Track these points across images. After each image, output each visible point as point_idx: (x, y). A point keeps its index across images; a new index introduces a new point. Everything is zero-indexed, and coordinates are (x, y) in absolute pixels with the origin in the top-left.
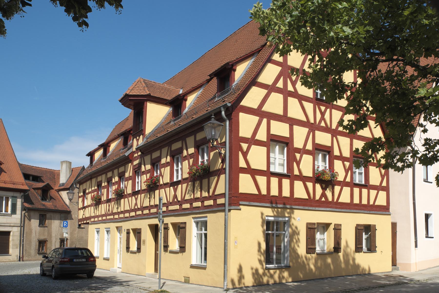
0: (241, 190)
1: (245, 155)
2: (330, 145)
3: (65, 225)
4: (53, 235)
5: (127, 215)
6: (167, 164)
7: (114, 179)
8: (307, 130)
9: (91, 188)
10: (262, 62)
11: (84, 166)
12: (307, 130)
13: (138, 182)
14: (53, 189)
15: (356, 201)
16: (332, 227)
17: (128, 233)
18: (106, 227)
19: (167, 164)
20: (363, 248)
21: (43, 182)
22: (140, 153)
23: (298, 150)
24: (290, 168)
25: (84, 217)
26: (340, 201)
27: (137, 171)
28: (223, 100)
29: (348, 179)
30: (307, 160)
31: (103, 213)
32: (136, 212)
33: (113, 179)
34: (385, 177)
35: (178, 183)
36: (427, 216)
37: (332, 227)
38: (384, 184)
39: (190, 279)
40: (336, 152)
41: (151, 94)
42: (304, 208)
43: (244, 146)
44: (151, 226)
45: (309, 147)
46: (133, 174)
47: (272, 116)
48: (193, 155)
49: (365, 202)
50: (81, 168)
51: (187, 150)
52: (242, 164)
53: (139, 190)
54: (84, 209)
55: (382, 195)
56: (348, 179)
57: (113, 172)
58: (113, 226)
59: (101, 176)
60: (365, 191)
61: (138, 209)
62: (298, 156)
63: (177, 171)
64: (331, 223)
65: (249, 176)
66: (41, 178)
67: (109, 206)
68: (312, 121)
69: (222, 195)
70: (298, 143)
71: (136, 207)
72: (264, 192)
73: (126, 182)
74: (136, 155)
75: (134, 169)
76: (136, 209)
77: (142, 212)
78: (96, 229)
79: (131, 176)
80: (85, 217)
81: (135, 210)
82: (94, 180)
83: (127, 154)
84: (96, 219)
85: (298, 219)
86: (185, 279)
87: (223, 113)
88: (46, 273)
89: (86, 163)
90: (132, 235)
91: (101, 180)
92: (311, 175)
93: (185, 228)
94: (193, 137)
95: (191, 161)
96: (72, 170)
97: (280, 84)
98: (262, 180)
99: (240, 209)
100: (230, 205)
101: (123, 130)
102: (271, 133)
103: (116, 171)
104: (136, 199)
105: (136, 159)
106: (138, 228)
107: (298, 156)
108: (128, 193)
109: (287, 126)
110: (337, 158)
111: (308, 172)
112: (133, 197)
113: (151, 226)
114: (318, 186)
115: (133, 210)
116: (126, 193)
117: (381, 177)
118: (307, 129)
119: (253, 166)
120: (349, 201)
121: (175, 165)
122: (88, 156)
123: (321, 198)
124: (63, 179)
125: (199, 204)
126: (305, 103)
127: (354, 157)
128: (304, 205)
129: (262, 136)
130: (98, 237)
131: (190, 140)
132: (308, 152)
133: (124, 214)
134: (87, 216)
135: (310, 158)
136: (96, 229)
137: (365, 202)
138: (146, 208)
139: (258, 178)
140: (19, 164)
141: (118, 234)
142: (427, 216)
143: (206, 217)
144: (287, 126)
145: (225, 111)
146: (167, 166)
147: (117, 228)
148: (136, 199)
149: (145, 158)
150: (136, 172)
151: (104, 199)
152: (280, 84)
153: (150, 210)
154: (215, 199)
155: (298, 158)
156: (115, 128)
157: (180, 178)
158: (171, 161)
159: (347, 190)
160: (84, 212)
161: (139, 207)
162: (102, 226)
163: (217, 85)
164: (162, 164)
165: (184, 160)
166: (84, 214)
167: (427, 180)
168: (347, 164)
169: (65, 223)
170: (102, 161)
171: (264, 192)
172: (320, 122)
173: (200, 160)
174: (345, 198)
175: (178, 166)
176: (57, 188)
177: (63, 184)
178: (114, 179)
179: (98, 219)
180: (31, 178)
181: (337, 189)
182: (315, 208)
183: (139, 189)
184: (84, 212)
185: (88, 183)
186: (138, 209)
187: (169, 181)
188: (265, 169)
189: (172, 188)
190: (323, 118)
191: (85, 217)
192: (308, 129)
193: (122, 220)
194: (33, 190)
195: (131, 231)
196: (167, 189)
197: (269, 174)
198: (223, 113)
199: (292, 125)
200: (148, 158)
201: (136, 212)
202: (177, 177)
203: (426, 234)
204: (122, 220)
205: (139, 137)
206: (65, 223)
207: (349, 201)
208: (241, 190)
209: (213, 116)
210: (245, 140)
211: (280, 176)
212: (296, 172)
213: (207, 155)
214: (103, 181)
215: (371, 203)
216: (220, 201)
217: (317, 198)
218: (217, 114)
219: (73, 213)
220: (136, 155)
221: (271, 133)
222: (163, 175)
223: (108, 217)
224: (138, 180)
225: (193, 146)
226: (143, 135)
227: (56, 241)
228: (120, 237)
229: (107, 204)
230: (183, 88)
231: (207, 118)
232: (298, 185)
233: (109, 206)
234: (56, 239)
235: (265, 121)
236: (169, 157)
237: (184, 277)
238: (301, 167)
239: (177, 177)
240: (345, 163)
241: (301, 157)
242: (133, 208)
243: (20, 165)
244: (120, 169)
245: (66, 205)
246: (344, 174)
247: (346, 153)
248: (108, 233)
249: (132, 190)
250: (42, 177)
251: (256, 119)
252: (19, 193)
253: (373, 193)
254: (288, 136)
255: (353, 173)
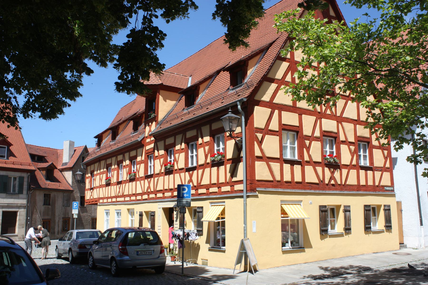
1: (260, 143)
2: (336, 131)
3: (75, 207)
4: (57, 214)
5: (139, 197)
6: (182, 150)
7: (125, 162)
9: (100, 170)
10: (273, 60)
11: (86, 146)
12: (314, 118)
13: (151, 166)
14: (57, 168)
15: (363, 182)
17: (141, 215)
18: (116, 209)
19: (182, 150)
20: (372, 228)
21: (47, 162)
22: (153, 139)
23: (307, 137)
24: (301, 155)
25: (92, 198)
26: (347, 183)
27: (150, 155)
28: (237, 93)
29: (354, 162)
30: (316, 146)
31: (113, 195)
32: (148, 195)
33: (124, 162)
35: (193, 169)
39: (208, 261)
40: (342, 138)
41: (164, 84)
43: (260, 136)
44: (165, 209)
45: (317, 134)
46: (145, 158)
47: (282, 108)
48: (208, 143)
50: (84, 147)
51: (202, 138)
52: (258, 153)
53: (153, 174)
54: (91, 191)
56: (354, 162)
57: (124, 156)
58: (124, 208)
59: (110, 159)
60: (370, 173)
61: (152, 193)
62: (307, 142)
63: (192, 157)
64: (341, 205)
66: (45, 158)
67: (119, 189)
69: (240, 182)
70: (307, 131)
71: (149, 191)
73: (138, 166)
74: (148, 140)
75: (147, 154)
76: (149, 192)
77: (156, 195)
78: (105, 210)
79: (143, 160)
80: (93, 198)
81: (148, 193)
82: (103, 163)
83: (139, 139)
84: (105, 201)
86: (203, 262)
87: (239, 107)
88: (97, 264)
89: (92, 144)
90: (145, 217)
91: (110, 162)
92: (319, 160)
93: (202, 212)
94: (208, 126)
95: (207, 148)
96: (75, 150)
98: (276, 166)
101: (131, 113)
102: (283, 123)
103: (127, 155)
104: (149, 183)
105: (150, 143)
106: (152, 211)
107: (307, 142)
108: (140, 176)
109: (296, 116)
110: (343, 142)
111: (317, 157)
112: (146, 181)
113: (165, 209)
114: (326, 169)
115: (145, 193)
116: (138, 177)
117: (385, 159)
120: (356, 183)
121: (189, 151)
122: (96, 138)
124: (66, 158)
125: (215, 189)
128: (315, 189)
129: (274, 126)
130: (108, 218)
131: (206, 129)
132: (317, 139)
133: (136, 197)
134: (95, 198)
136: (105, 210)
137: (370, 183)
138: (160, 191)
139: (272, 164)
140: (25, 144)
141: (130, 216)
143: (224, 202)
146: (182, 152)
147: (128, 210)
148: (149, 183)
149: (158, 143)
150: (148, 156)
151: (114, 182)
152: (288, 78)
153: (163, 194)
154: (232, 186)
155: (308, 145)
156: (121, 110)
157: (195, 164)
158: (186, 147)
159: (353, 172)
160: (92, 193)
161: (152, 190)
162: (112, 208)
163: (229, 77)
164: (176, 150)
165: (200, 147)
166: (91, 195)
168: (352, 148)
169: (75, 205)
170: (111, 143)
173: (216, 148)
174: (352, 180)
175: (192, 152)
176: (60, 167)
177: (66, 164)
178: (125, 162)
179: (107, 201)
180: (36, 158)
181: (345, 171)
183: (152, 173)
184: (92, 193)
185: (96, 165)
186: (152, 193)
187: (184, 167)
188: (278, 156)
189: (187, 173)
191: (93, 198)
192: (315, 117)
193: (134, 202)
194: (38, 170)
195: (144, 214)
196: (182, 174)
197: (282, 160)
198: (239, 107)
200: (161, 144)
201: (148, 195)
202: (192, 164)
204: (134, 202)
205: (152, 123)
206: (75, 205)
207: (356, 183)
209: (230, 110)
210: (259, 130)
211: (292, 163)
212: (306, 158)
213: (223, 144)
214: (113, 163)
215: (377, 184)
216: (237, 187)
217: (327, 182)
218: (233, 107)
219: (76, 192)
220: (148, 140)
221: (283, 123)
222: (177, 160)
223: (119, 199)
224: (151, 164)
225: (209, 135)
226: (156, 121)
227: (59, 221)
228: (132, 219)
229: (118, 186)
230: (191, 76)
231: (224, 111)
232: (309, 169)
233: (119, 189)
234: (59, 218)
235: (276, 112)
236: (183, 144)
237: (202, 259)
238: (311, 153)
239: (192, 164)
240: (351, 147)
241: (310, 144)
242: (145, 191)
243: (27, 145)
244: (131, 153)
245: (69, 184)
246: (350, 157)
247: (351, 139)
248: (118, 215)
249: (145, 173)
250: (46, 157)
252: (26, 173)
253: (378, 174)
254: (298, 125)
255: (359, 157)
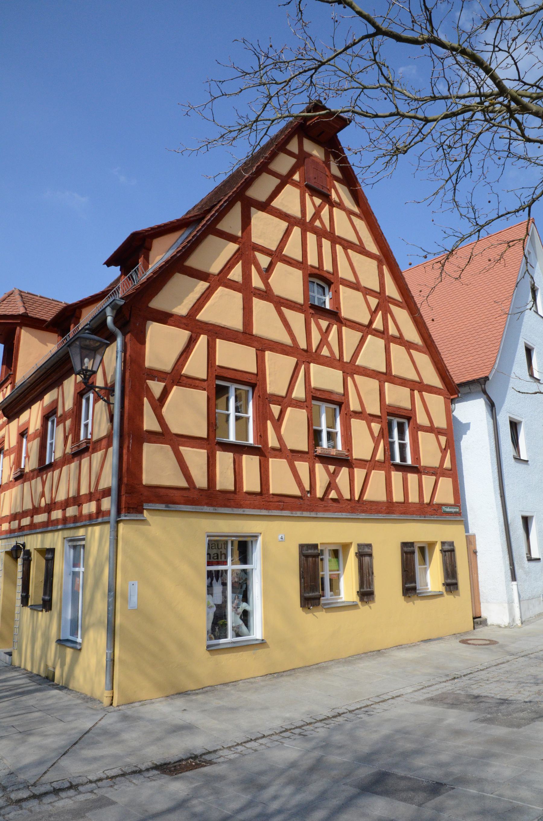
0: (147, 479)
1: (278, 423)
8: (293, 361)
12: (293, 361)
16: (353, 551)
34: (380, 441)
36: (526, 521)
37: (353, 551)
38: (447, 464)
40: (354, 405)
42: (244, 511)
45: (299, 392)
49: (413, 498)
55: (445, 484)
60: (412, 478)
64: (351, 543)
65: (284, 462)
68: (303, 345)
72: (201, 481)
85: (280, 537)
97: (236, 274)
99: (144, 521)
100: (119, 513)
107: (275, 409)
110: (359, 415)
118: (295, 360)
119: (175, 429)
123: (327, 492)
126: (288, 313)
127: (388, 415)
135: (303, 414)
142: (526, 521)
144: (252, 351)
145: (114, 315)
152: (236, 274)
167: (520, 457)
171: (201, 481)
172: (319, 347)
182: (302, 514)
190: (324, 341)
199: (310, 362)
203: (527, 554)
208: (147, 479)
210: (155, 374)
212: (272, 441)
217: (319, 493)
235: (203, 339)
246: (372, 445)
247: (374, 408)
251: (184, 335)
253: (428, 481)
